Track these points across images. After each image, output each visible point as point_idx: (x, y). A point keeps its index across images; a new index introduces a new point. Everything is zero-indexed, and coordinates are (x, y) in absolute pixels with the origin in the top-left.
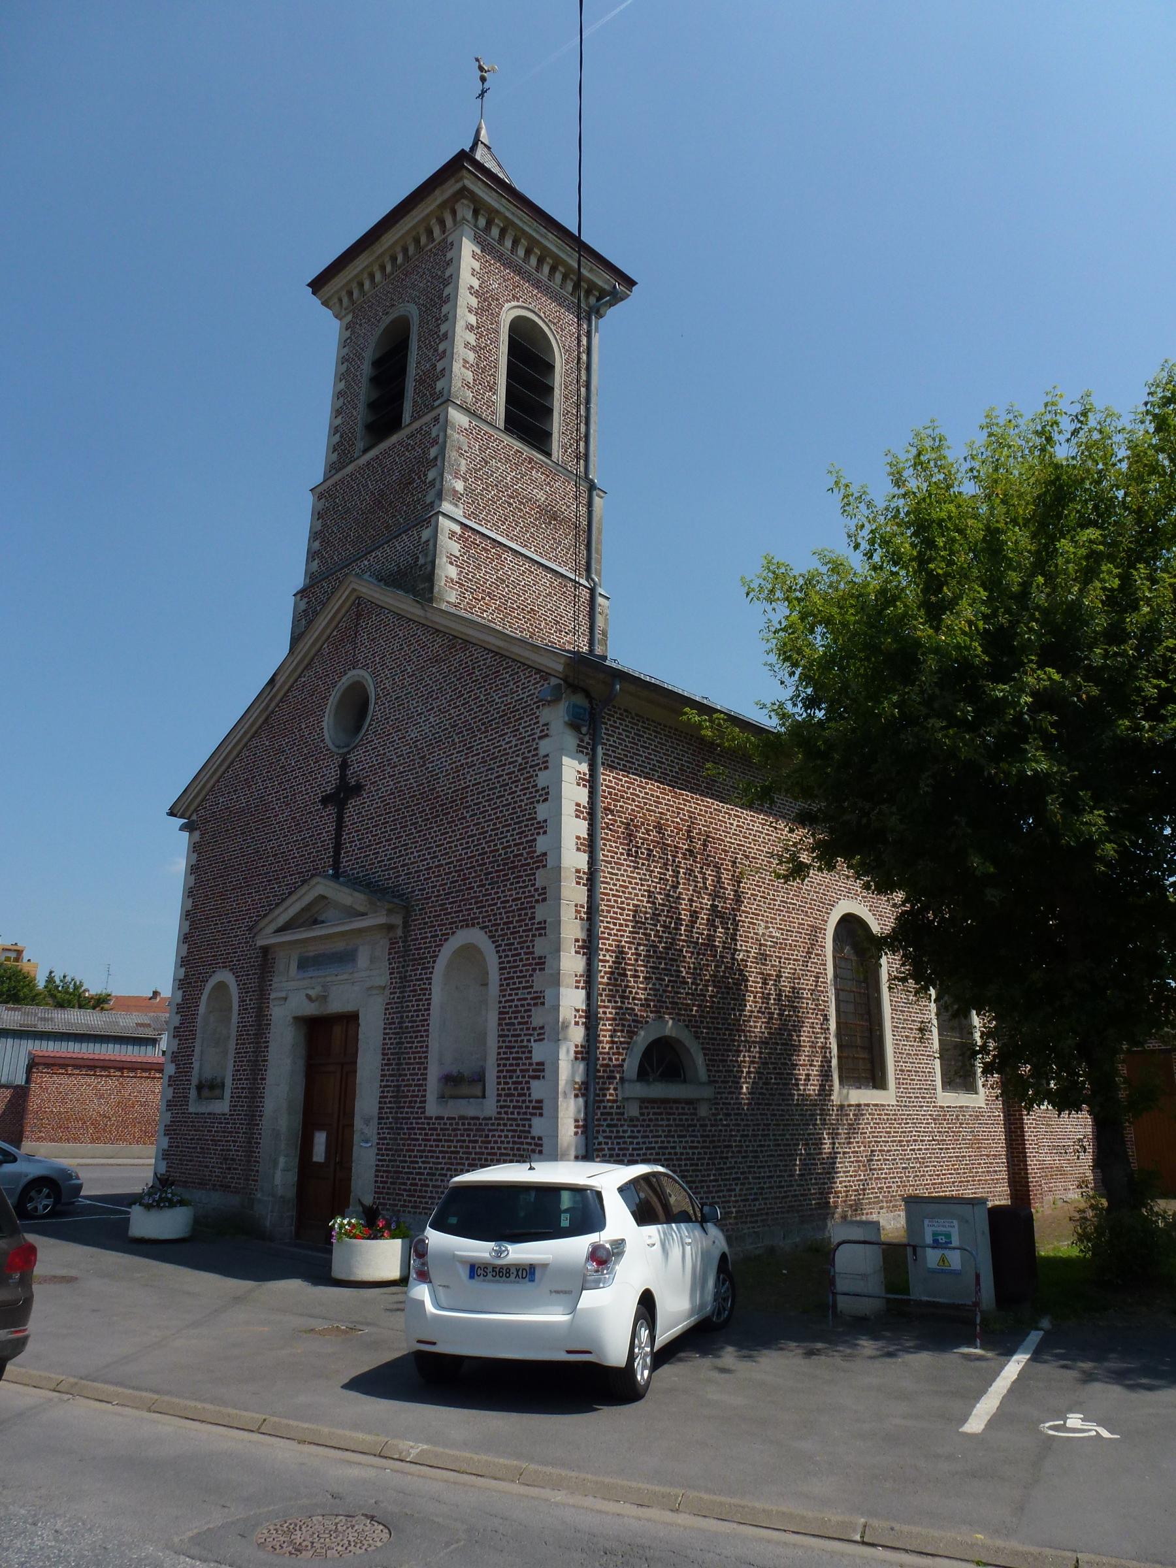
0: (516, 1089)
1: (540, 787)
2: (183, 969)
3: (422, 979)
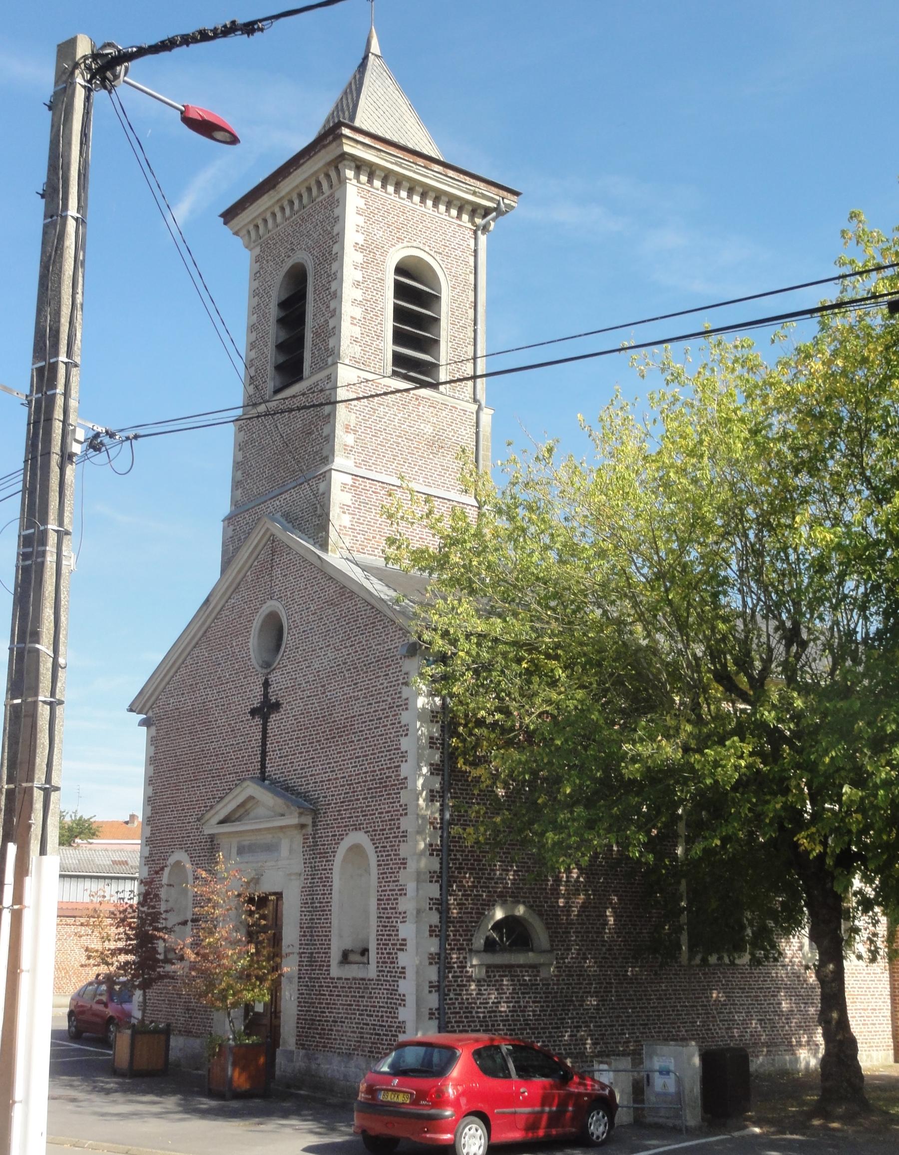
0: (389, 958)
1: (403, 723)
2: (148, 848)
3: (326, 870)
